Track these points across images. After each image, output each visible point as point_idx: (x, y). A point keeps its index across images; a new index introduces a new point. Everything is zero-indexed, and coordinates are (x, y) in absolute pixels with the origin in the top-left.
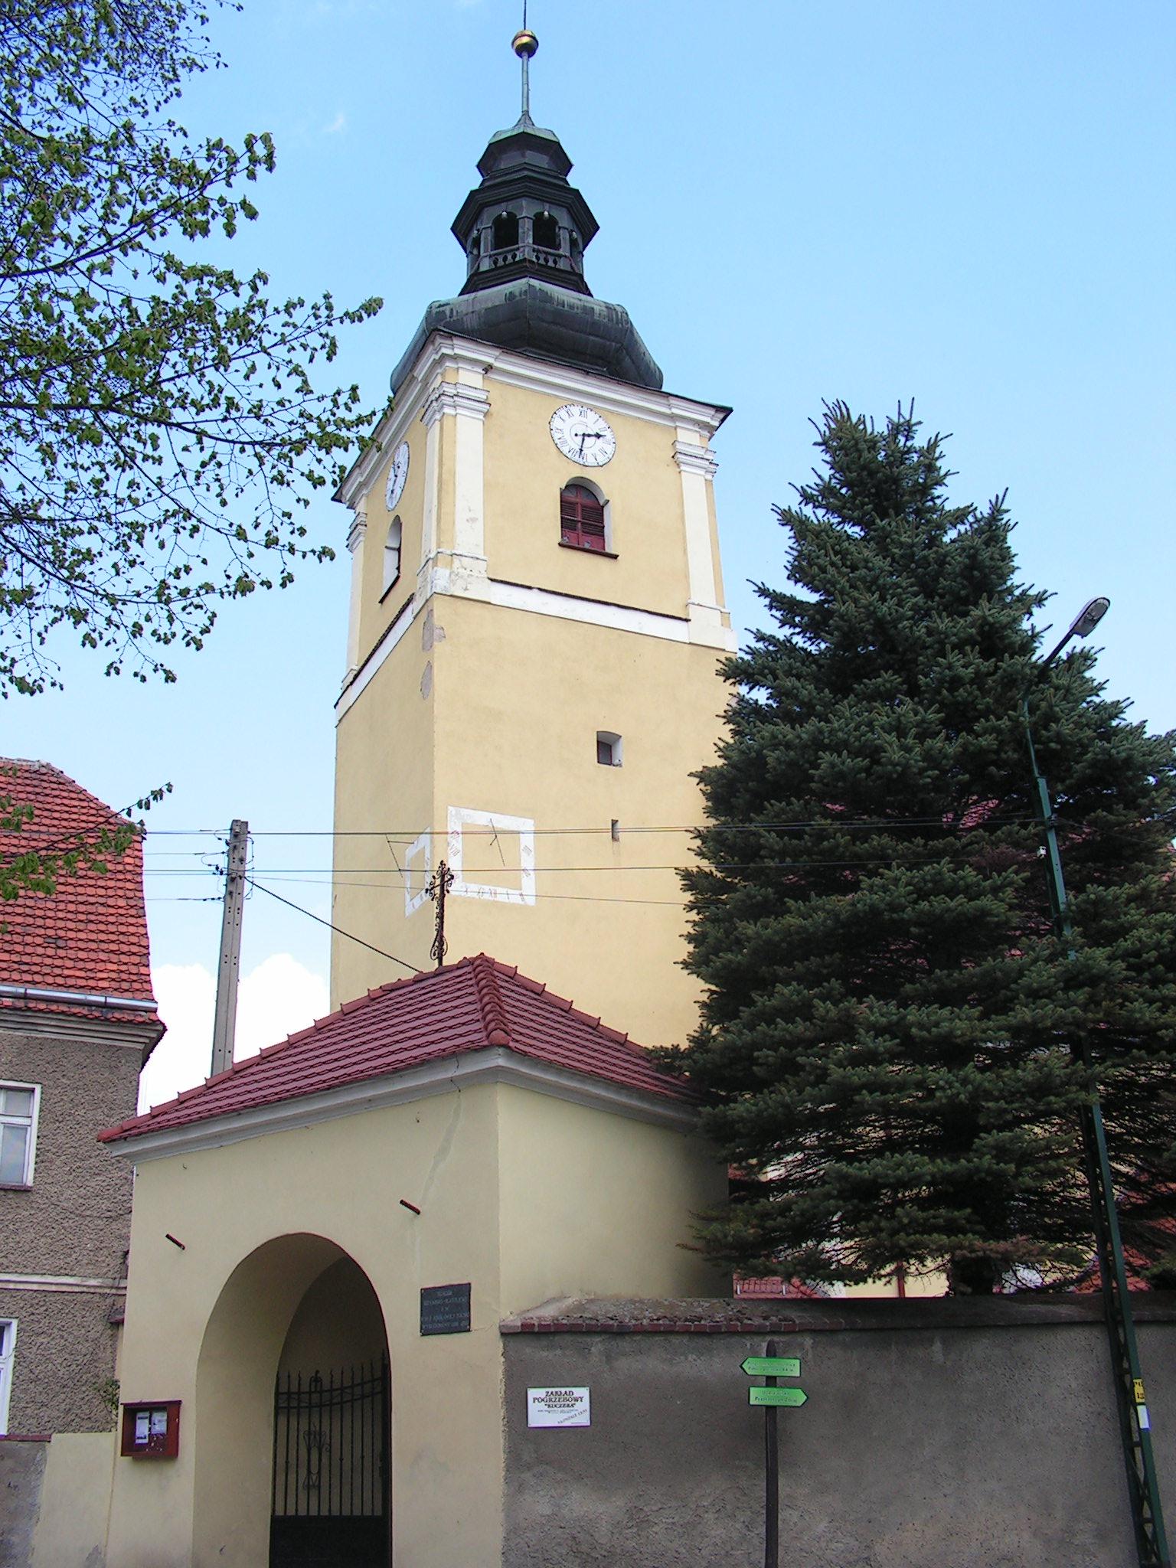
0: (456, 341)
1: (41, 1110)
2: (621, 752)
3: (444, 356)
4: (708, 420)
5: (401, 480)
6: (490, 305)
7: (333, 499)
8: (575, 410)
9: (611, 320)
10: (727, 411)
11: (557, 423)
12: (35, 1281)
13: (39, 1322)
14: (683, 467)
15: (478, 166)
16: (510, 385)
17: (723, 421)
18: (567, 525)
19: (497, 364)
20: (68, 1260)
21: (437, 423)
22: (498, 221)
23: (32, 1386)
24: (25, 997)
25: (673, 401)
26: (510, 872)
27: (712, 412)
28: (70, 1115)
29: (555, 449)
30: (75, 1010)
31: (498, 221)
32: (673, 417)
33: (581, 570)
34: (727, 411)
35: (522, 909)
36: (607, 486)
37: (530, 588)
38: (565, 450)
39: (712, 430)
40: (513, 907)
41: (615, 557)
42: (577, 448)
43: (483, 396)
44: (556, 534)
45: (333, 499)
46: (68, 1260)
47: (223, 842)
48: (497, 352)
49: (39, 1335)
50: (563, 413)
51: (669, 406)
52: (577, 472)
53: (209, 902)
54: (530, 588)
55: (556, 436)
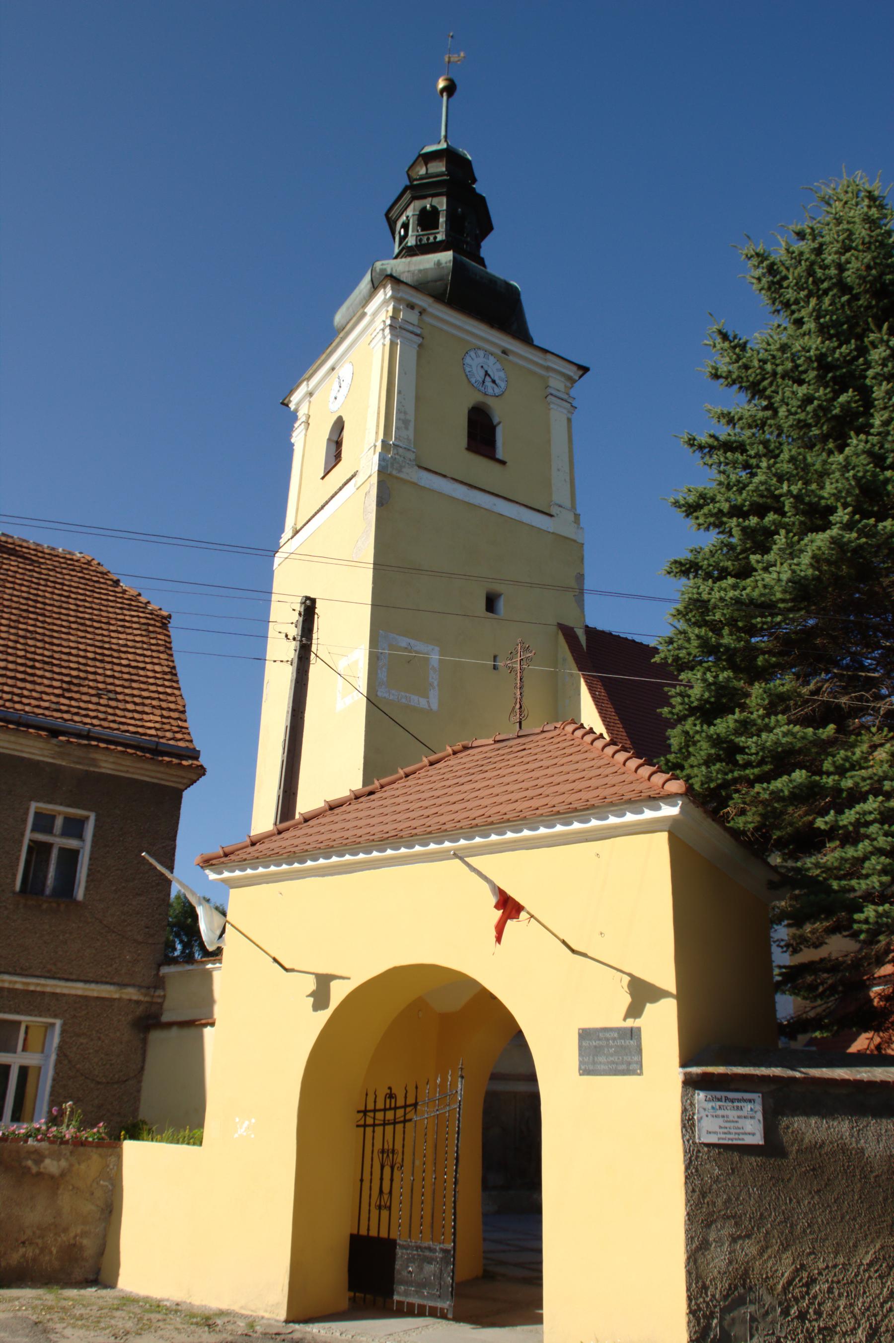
2: (501, 604)
4: (571, 374)
5: (345, 390)
8: (481, 353)
10: (585, 370)
11: (468, 360)
12: (78, 989)
14: (552, 406)
17: (580, 377)
18: (471, 436)
19: (430, 310)
22: (423, 210)
25: (549, 356)
27: (574, 368)
31: (423, 210)
32: (548, 369)
33: (479, 467)
34: (585, 370)
36: (499, 412)
38: (473, 380)
39: (573, 381)
41: (503, 463)
42: (481, 380)
43: (418, 331)
46: (109, 969)
47: (297, 613)
50: (472, 354)
52: (479, 398)
53: (278, 663)
55: (468, 369)
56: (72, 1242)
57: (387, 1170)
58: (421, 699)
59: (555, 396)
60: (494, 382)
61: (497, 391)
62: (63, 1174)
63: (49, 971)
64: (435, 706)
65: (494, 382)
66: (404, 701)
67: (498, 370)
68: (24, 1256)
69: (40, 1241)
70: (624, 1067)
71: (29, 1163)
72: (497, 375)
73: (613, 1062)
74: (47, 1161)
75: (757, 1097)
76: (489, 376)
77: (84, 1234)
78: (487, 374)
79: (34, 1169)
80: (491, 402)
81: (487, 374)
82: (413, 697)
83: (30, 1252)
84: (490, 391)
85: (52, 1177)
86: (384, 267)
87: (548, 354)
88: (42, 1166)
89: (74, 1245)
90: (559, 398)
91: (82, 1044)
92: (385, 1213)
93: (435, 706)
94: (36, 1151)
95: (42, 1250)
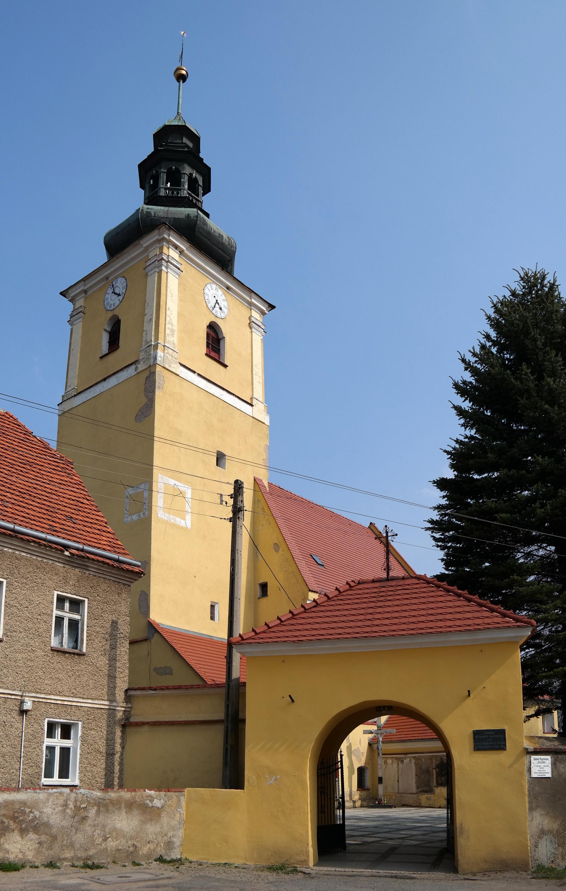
0: (172, 233)
1: (88, 613)
3: (164, 239)
6: (176, 217)
7: (61, 293)
9: (229, 244)
11: (206, 291)
13: (91, 723)
15: (154, 135)
16: (188, 263)
19: (186, 251)
20: (103, 692)
21: (156, 274)
23: (89, 756)
24: (82, 550)
25: (253, 295)
26: (181, 513)
28: (101, 616)
29: (205, 305)
30: (108, 561)
33: (210, 367)
34: (272, 307)
35: (185, 529)
36: (226, 329)
37: (194, 372)
40: (182, 528)
44: (204, 349)
45: (61, 293)
46: (103, 692)
48: (188, 245)
49: (91, 730)
51: (251, 298)
53: (223, 520)
54: (194, 372)
55: (206, 298)
56: (169, 840)
57: (323, 795)
58: (182, 521)
59: (255, 324)
60: (221, 309)
61: (223, 316)
62: (163, 807)
63: (73, 693)
64: (189, 526)
65: (221, 309)
66: (172, 521)
67: (223, 300)
68: (149, 848)
69: (155, 841)
70: (498, 747)
71: (148, 801)
72: (223, 304)
73: (492, 745)
74: (155, 800)
75: (549, 757)
76: (218, 304)
77: (174, 836)
78: (217, 302)
79: (150, 805)
80: (220, 323)
81: (217, 302)
82: (177, 519)
83: (152, 846)
84: (219, 315)
85: (158, 808)
86: (149, 210)
87: (252, 293)
88: (154, 802)
89: (170, 842)
90: (257, 325)
91: (93, 734)
92: (323, 814)
93: (189, 526)
94: (150, 796)
95: (157, 845)
